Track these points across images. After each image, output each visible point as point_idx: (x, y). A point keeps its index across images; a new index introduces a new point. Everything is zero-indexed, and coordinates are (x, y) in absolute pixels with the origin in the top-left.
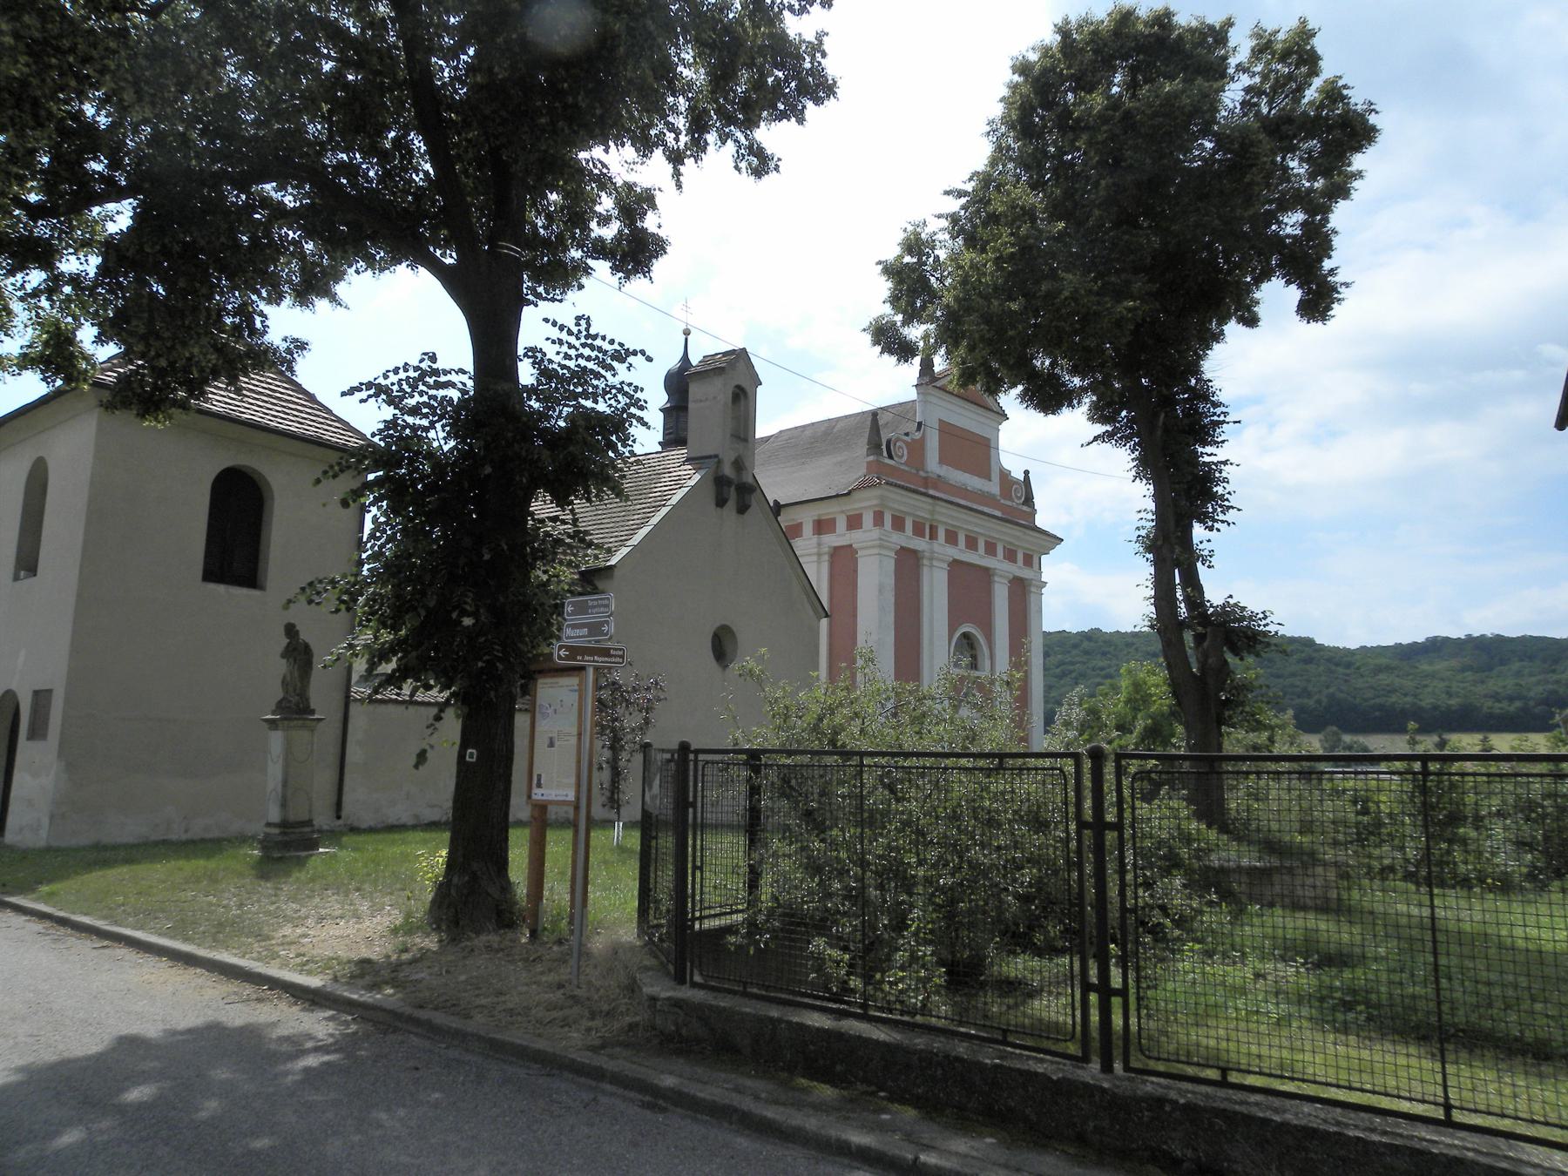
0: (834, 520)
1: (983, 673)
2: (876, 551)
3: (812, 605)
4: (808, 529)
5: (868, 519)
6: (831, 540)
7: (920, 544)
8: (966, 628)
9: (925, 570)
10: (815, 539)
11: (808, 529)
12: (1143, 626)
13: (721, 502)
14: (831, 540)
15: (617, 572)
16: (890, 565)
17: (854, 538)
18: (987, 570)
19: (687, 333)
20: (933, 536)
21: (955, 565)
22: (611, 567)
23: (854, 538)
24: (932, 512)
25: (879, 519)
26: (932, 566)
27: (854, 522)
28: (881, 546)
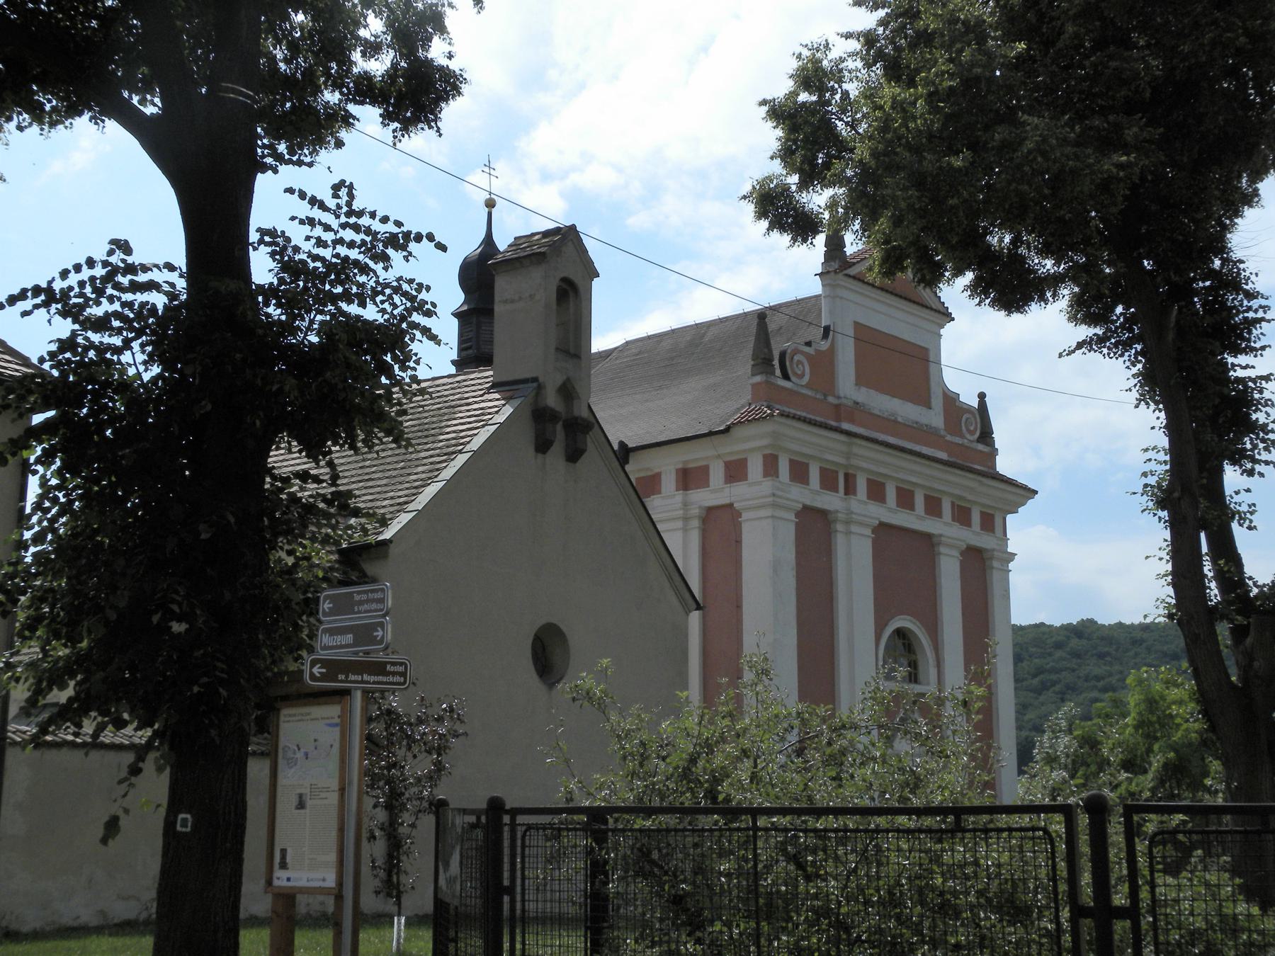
2: (768, 512)
4: (669, 482)
5: (755, 467)
6: (704, 497)
7: (831, 501)
9: (840, 541)
10: (679, 497)
11: (669, 482)
14: (704, 497)
15: (393, 550)
17: (737, 494)
20: (850, 489)
21: (883, 531)
22: (385, 543)
23: (737, 494)
24: (848, 456)
25: (770, 466)
26: (849, 533)
27: (736, 471)
28: (774, 505)
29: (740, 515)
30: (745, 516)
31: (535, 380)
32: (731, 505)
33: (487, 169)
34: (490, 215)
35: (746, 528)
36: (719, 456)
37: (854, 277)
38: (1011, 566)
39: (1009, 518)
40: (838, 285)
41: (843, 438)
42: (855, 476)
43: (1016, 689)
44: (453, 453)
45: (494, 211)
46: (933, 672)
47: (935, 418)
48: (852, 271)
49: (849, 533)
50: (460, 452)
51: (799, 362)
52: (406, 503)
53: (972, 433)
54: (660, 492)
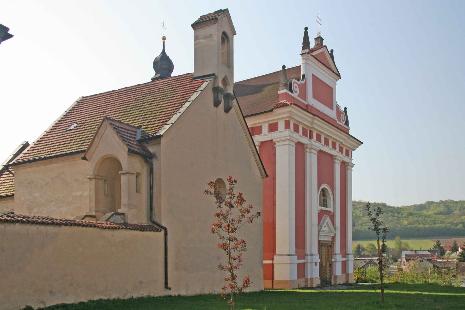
0: (261, 127)
1: (330, 209)
2: (287, 142)
3: (259, 169)
5: (281, 125)
7: (305, 140)
8: (324, 186)
9: (308, 155)
12: (353, 200)
13: (216, 104)
15: (163, 141)
16: (293, 149)
17: (273, 136)
18: (332, 156)
19: (164, 38)
20: (311, 137)
21: (321, 152)
22: (160, 136)
23: (273, 136)
24: (312, 123)
25: (287, 126)
26: (311, 152)
27: (273, 128)
28: (290, 140)
29: (275, 144)
30: (277, 144)
31: (213, 75)
32: (272, 140)
33: (162, 25)
34: (164, 42)
35: (277, 148)
36: (266, 122)
37: (313, 56)
38: (353, 168)
39: (353, 152)
40: (308, 59)
41: (311, 116)
42: (313, 132)
43: (368, 205)
44: (183, 102)
45: (165, 41)
46: (332, 203)
47: (332, 114)
48: (314, 54)
49: (311, 152)
50: (186, 102)
51: (296, 87)
52: (165, 121)
53: (343, 121)
54: (278, 130)
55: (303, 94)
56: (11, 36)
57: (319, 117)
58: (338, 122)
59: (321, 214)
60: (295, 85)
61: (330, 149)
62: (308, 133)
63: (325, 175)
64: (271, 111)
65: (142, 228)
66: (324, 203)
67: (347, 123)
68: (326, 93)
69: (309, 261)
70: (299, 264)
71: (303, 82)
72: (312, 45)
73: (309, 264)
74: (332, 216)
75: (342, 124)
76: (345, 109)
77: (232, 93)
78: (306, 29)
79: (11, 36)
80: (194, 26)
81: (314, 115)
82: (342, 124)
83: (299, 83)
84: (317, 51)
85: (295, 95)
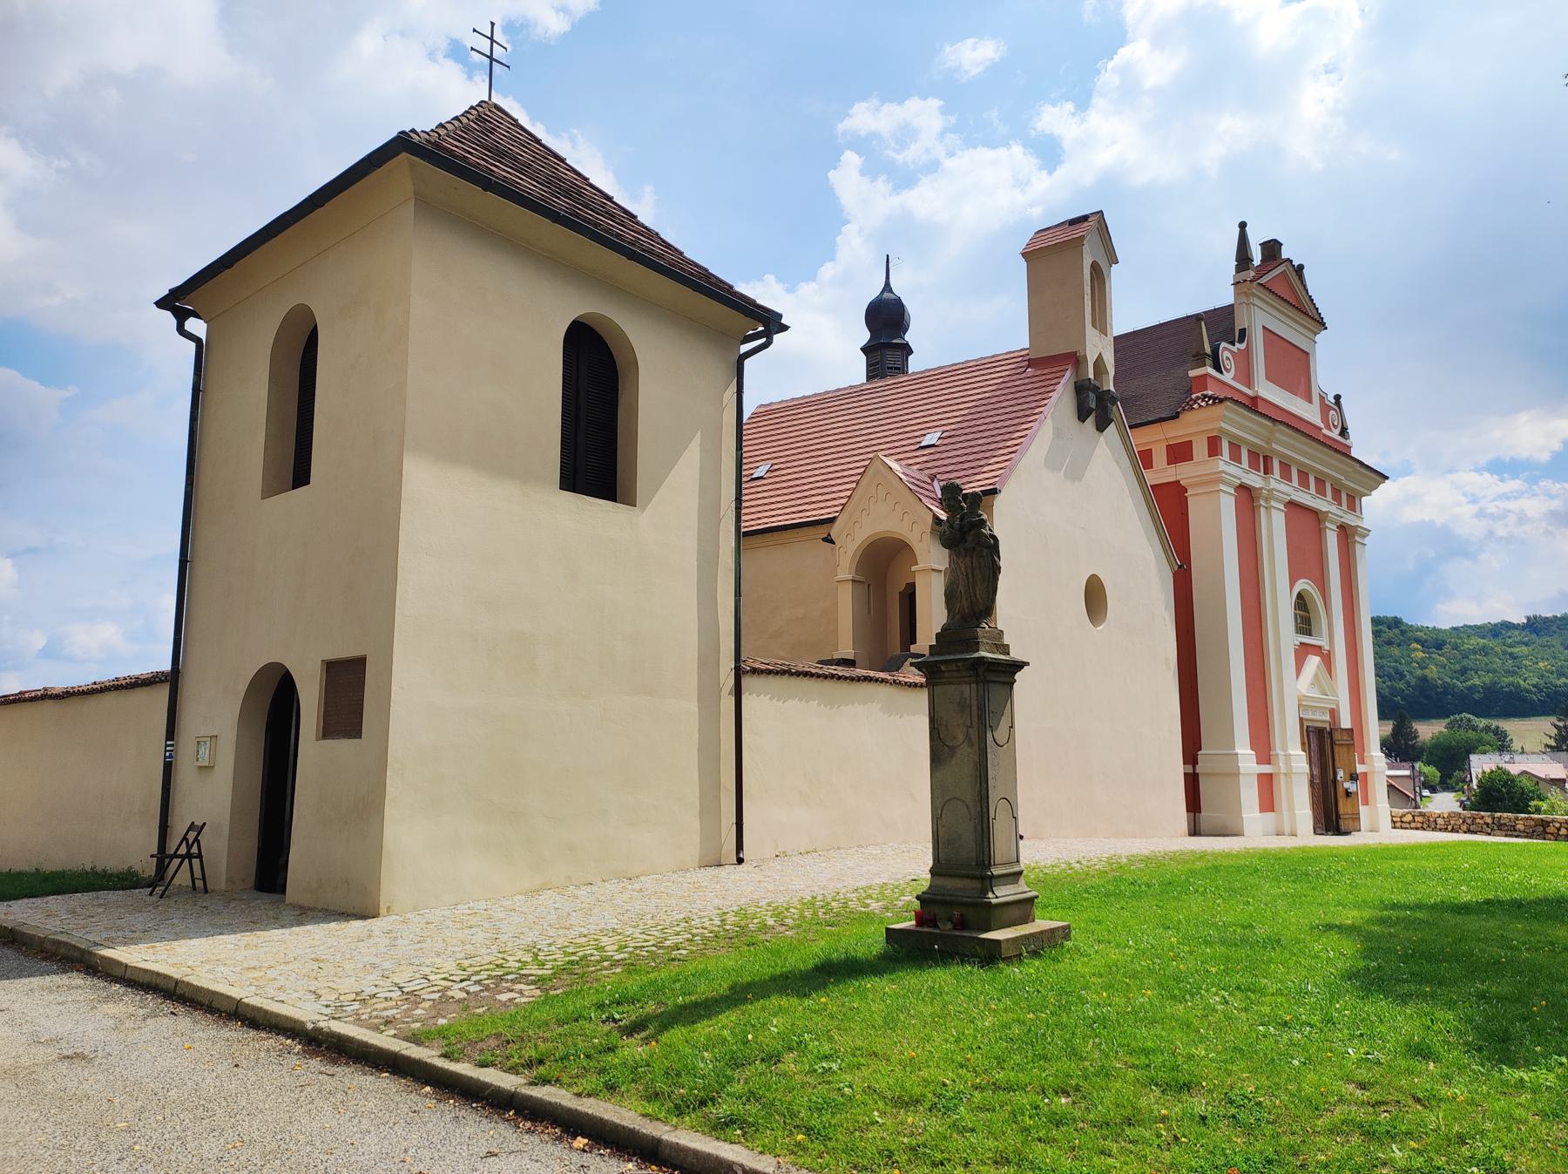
1: (1322, 642)
5: (1200, 450)
7: (1254, 480)
18: (1315, 513)
21: (1292, 504)
25: (1214, 448)
38: (1366, 541)
47: (1309, 412)
48: (1263, 281)
55: (1247, 376)
56: (161, 304)
57: (1287, 425)
58: (1325, 431)
59: (1303, 651)
60: (1226, 354)
61: (1314, 497)
62: (1261, 461)
63: (1306, 560)
64: (1177, 416)
65: (738, 528)
66: (1305, 623)
67: (1344, 432)
68: (1294, 367)
69: (1283, 770)
70: (1260, 775)
71: (1243, 346)
72: (1257, 257)
73: (1282, 778)
74: (1327, 660)
75: (1335, 434)
76: (1337, 398)
77: (1112, 389)
78: (1243, 225)
79: (161, 304)
80: (177, 302)
81: (1274, 421)
82: (1335, 434)
83: (1234, 349)
84: (1268, 271)
85: (1227, 377)
